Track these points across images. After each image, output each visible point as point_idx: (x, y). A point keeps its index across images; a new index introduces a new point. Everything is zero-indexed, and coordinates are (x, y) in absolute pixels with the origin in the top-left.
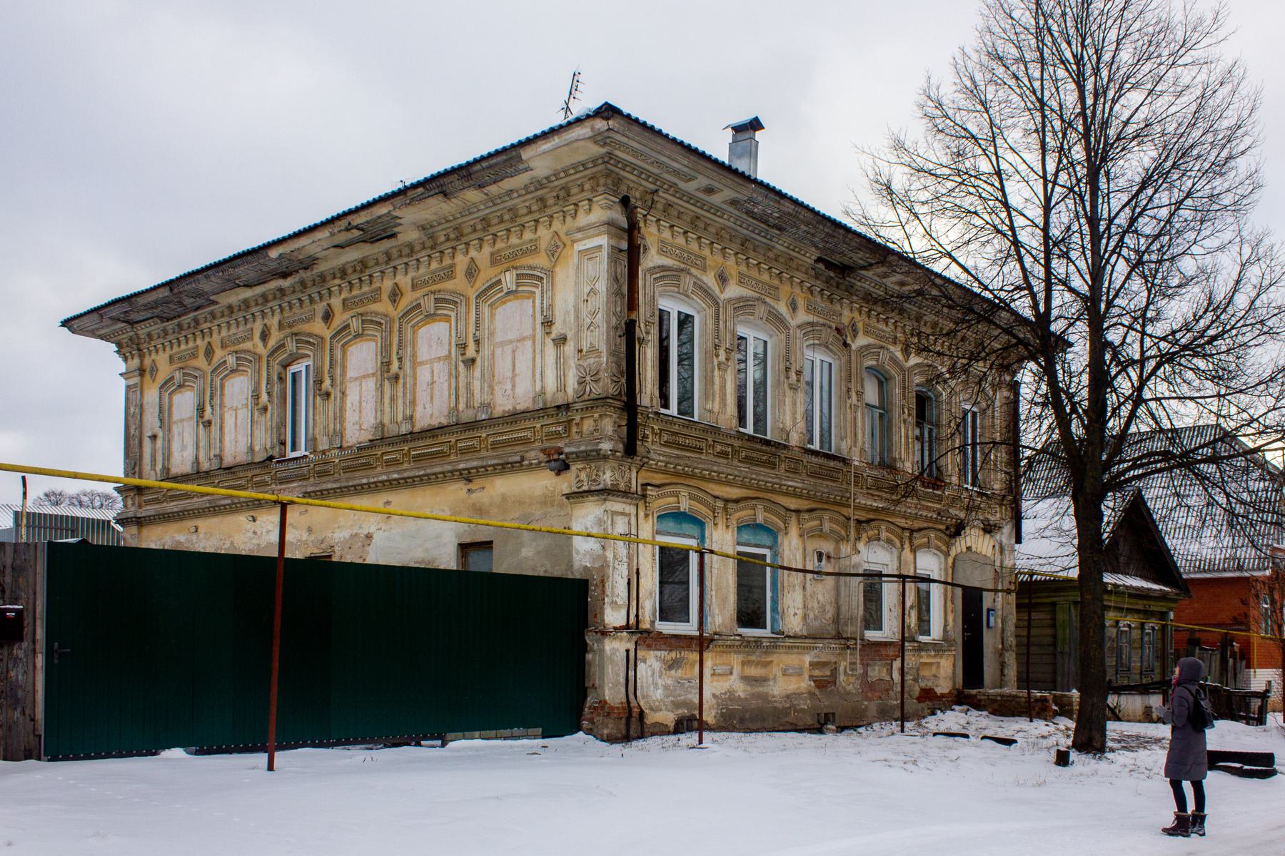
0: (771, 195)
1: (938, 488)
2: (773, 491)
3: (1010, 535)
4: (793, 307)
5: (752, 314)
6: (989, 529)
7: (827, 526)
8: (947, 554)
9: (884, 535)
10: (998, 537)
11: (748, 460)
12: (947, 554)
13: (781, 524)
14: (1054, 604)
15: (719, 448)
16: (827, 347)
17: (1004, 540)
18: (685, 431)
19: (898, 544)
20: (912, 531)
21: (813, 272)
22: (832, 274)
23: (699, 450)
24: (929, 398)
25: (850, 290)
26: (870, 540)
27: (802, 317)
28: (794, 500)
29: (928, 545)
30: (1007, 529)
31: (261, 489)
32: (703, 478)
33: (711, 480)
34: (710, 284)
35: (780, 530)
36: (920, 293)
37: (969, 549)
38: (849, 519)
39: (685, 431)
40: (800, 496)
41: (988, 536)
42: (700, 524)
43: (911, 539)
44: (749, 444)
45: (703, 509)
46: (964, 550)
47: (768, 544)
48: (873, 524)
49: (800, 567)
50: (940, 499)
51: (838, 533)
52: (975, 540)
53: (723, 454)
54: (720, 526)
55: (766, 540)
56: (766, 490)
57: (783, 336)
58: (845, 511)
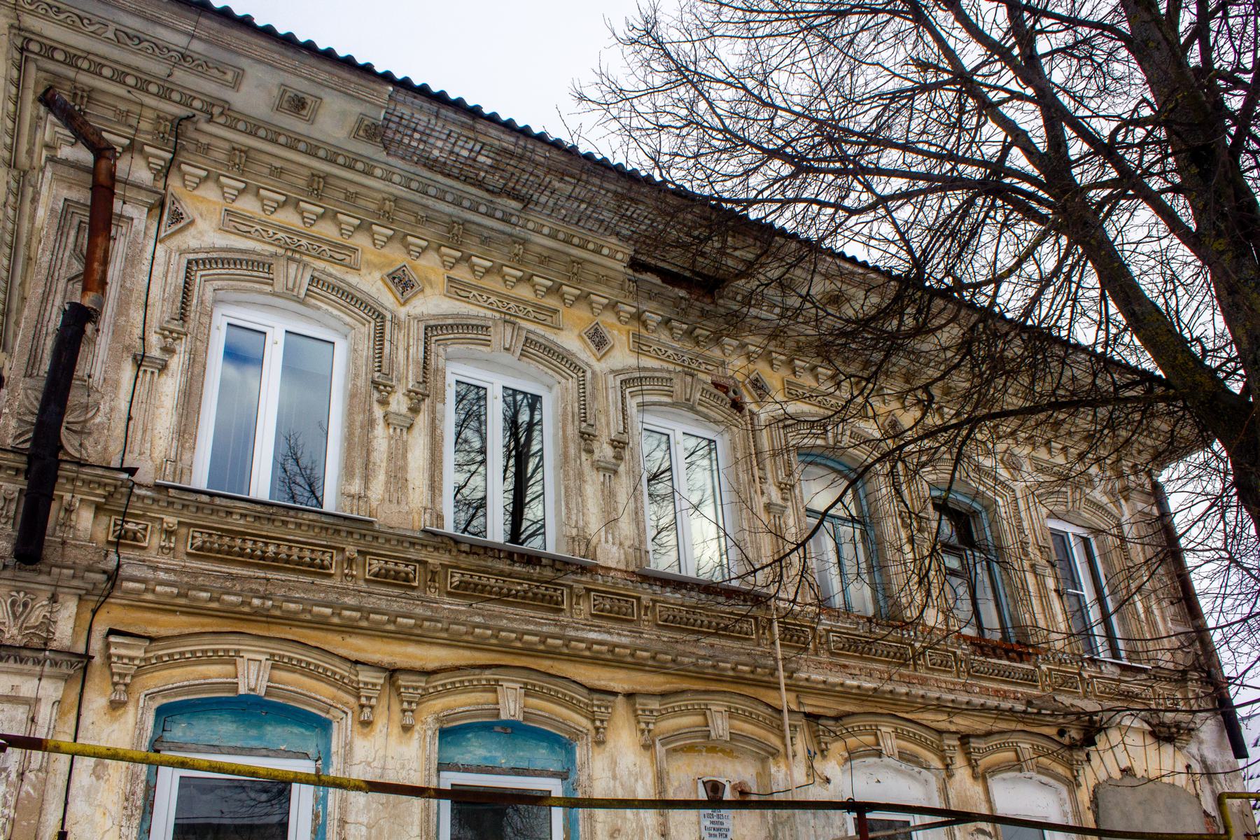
0: (449, 113)
1: (1021, 657)
2: (552, 654)
3: (1220, 745)
4: (599, 340)
5: (487, 343)
6: (1165, 734)
7: (721, 726)
8: (1073, 784)
9: (890, 743)
10: (1193, 748)
11: (464, 591)
12: (1073, 784)
13: (584, 723)
14: (465, 530)
15: (376, 565)
16: (692, 409)
17: (1210, 756)
18: (267, 529)
19: (936, 762)
20: (964, 739)
21: (632, 287)
22: (682, 293)
23: (321, 570)
24: (976, 514)
25: (735, 323)
26: (851, 755)
27: (622, 357)
28: (621, 674)
29: (1017, 765)
30: (1208, 729)
31: (236, 784)
32: (321, 624)
33: (349, 629)
34: (373, 291)
35: (577, 734)
36: (984, 443)
37: (1127, 772)
38: (780, 712)
39: (267, 529)
40: (638, 666)
41: (1168, 749)
42: (322, 726)
43: (967, 754)
44: (473, 560)
45: (324, 691)
46: (1116, 775)
47: (555, 766)
48: (852, 723)
49: (676, 815)
50: (1030, 679)
51: (759, 743)
52: (1127, 750)
53: (382, 578)
54: (380, 723)
55: (542, 756)
56: (529, 651)
57: (572, 384)
58: (770, 697)
